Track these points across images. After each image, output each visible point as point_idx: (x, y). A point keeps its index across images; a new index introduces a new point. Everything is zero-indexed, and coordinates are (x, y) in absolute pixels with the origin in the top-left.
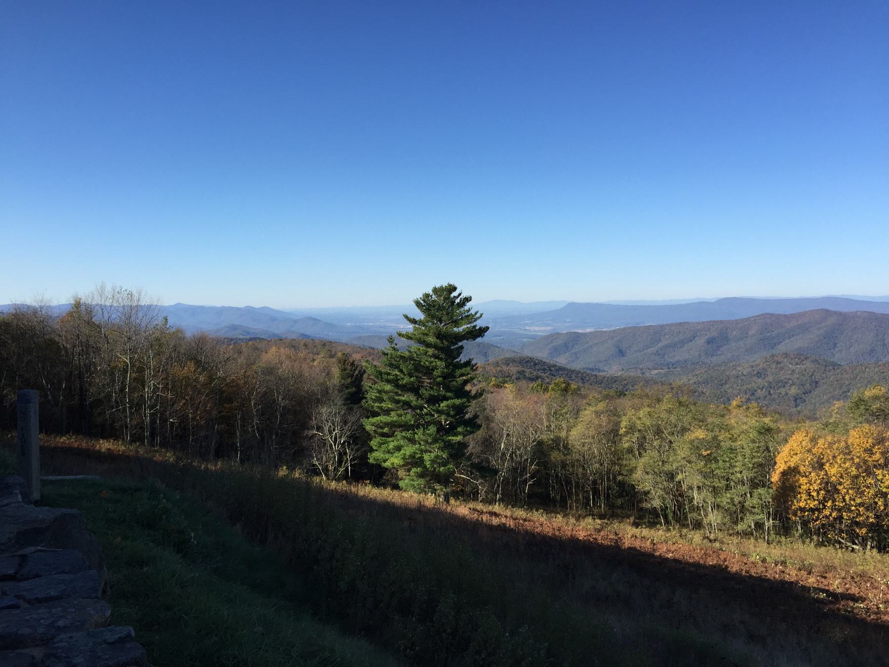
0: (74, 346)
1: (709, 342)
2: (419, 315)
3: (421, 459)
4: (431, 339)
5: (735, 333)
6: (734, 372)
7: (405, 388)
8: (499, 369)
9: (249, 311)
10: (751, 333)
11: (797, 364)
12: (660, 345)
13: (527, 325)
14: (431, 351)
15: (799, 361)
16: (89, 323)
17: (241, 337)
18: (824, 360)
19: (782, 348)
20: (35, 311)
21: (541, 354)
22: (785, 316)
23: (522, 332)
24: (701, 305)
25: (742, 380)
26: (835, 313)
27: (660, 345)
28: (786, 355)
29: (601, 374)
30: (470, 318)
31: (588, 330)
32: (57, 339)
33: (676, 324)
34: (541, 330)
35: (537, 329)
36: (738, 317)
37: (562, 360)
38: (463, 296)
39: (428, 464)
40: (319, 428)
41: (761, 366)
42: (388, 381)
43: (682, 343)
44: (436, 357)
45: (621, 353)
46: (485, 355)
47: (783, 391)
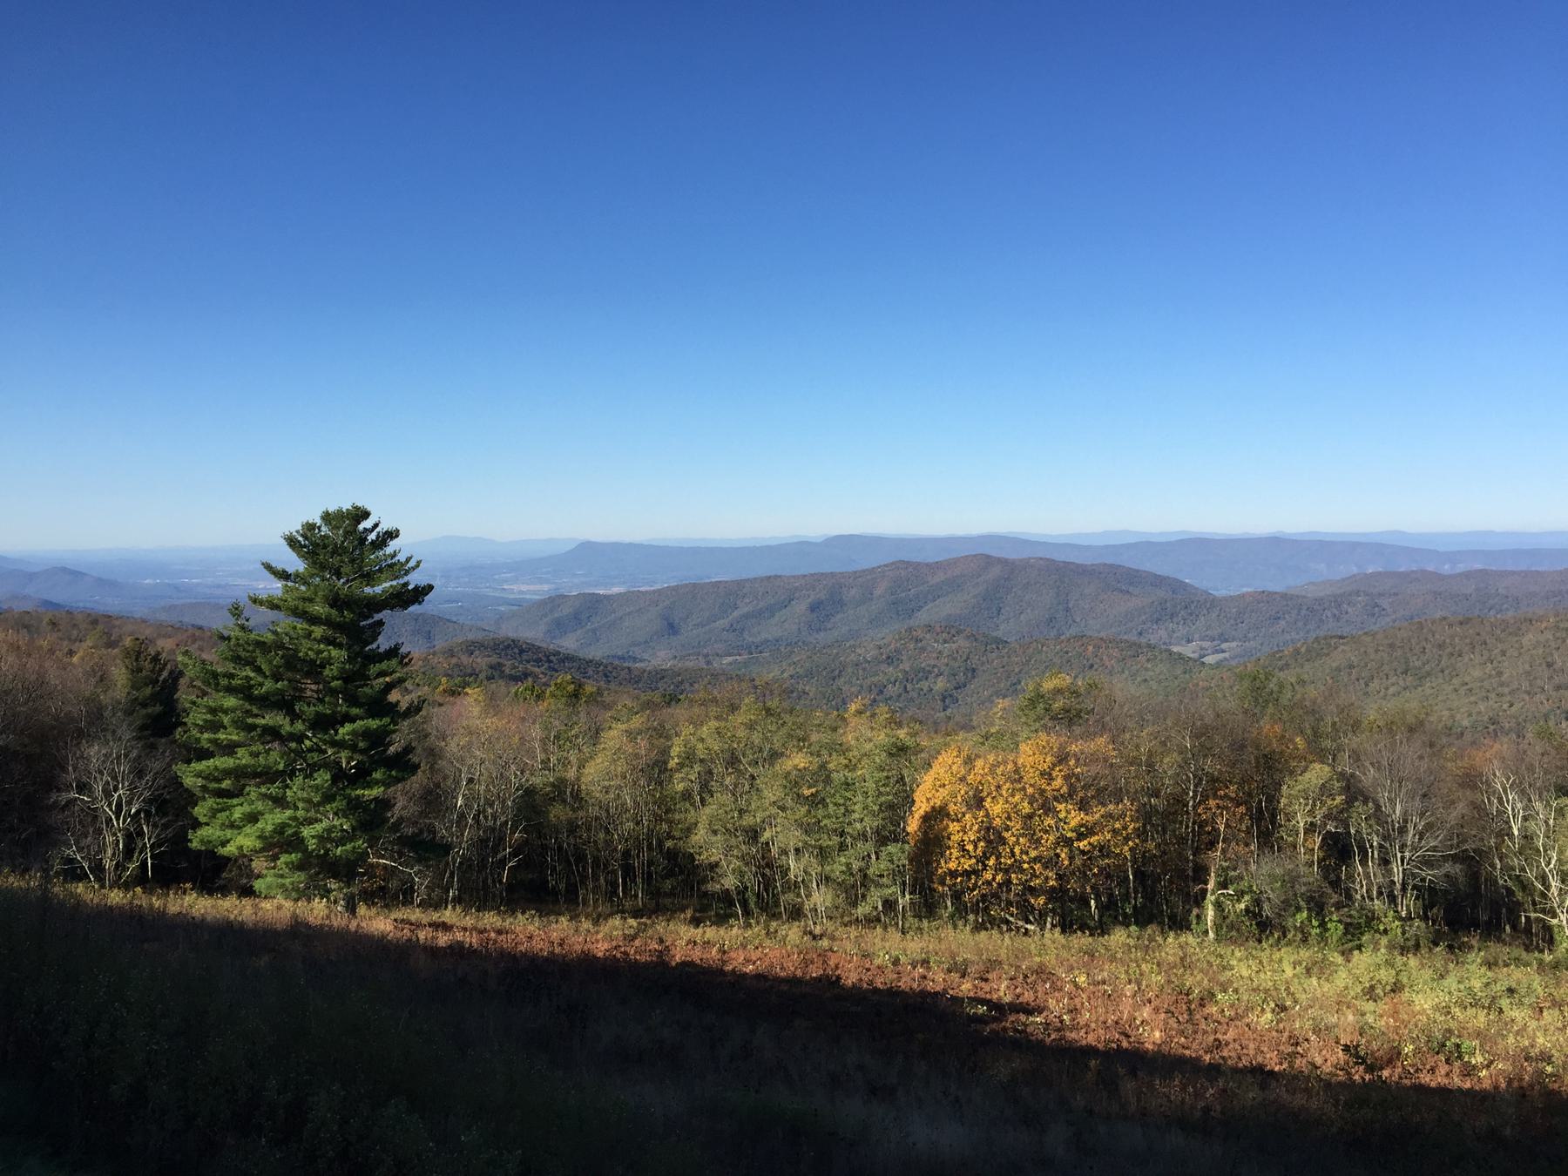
5: (853, 592)
6: (853, 657)
7: (266, 702)
8: (454, 660)
10: (877, 592)
11: (945, 642)
12: (736, 614)
13: (506, 581)
14: (318, 631)
19: (923, 617)
21: (533, 634)
24: (802, 548)
28: (929, 628)
30: (397, 568)
31: (616, 590)
33: (762, 579)
34: (532, 590)
35: (524, 588)
36: (858, 567)
37: (569, 643)
39: (312, 844)
40: (83, 788)
42: (230, 690)
43: (771, 610)
45: (672, 629)
46: (429, 636)
47: (925, 685)
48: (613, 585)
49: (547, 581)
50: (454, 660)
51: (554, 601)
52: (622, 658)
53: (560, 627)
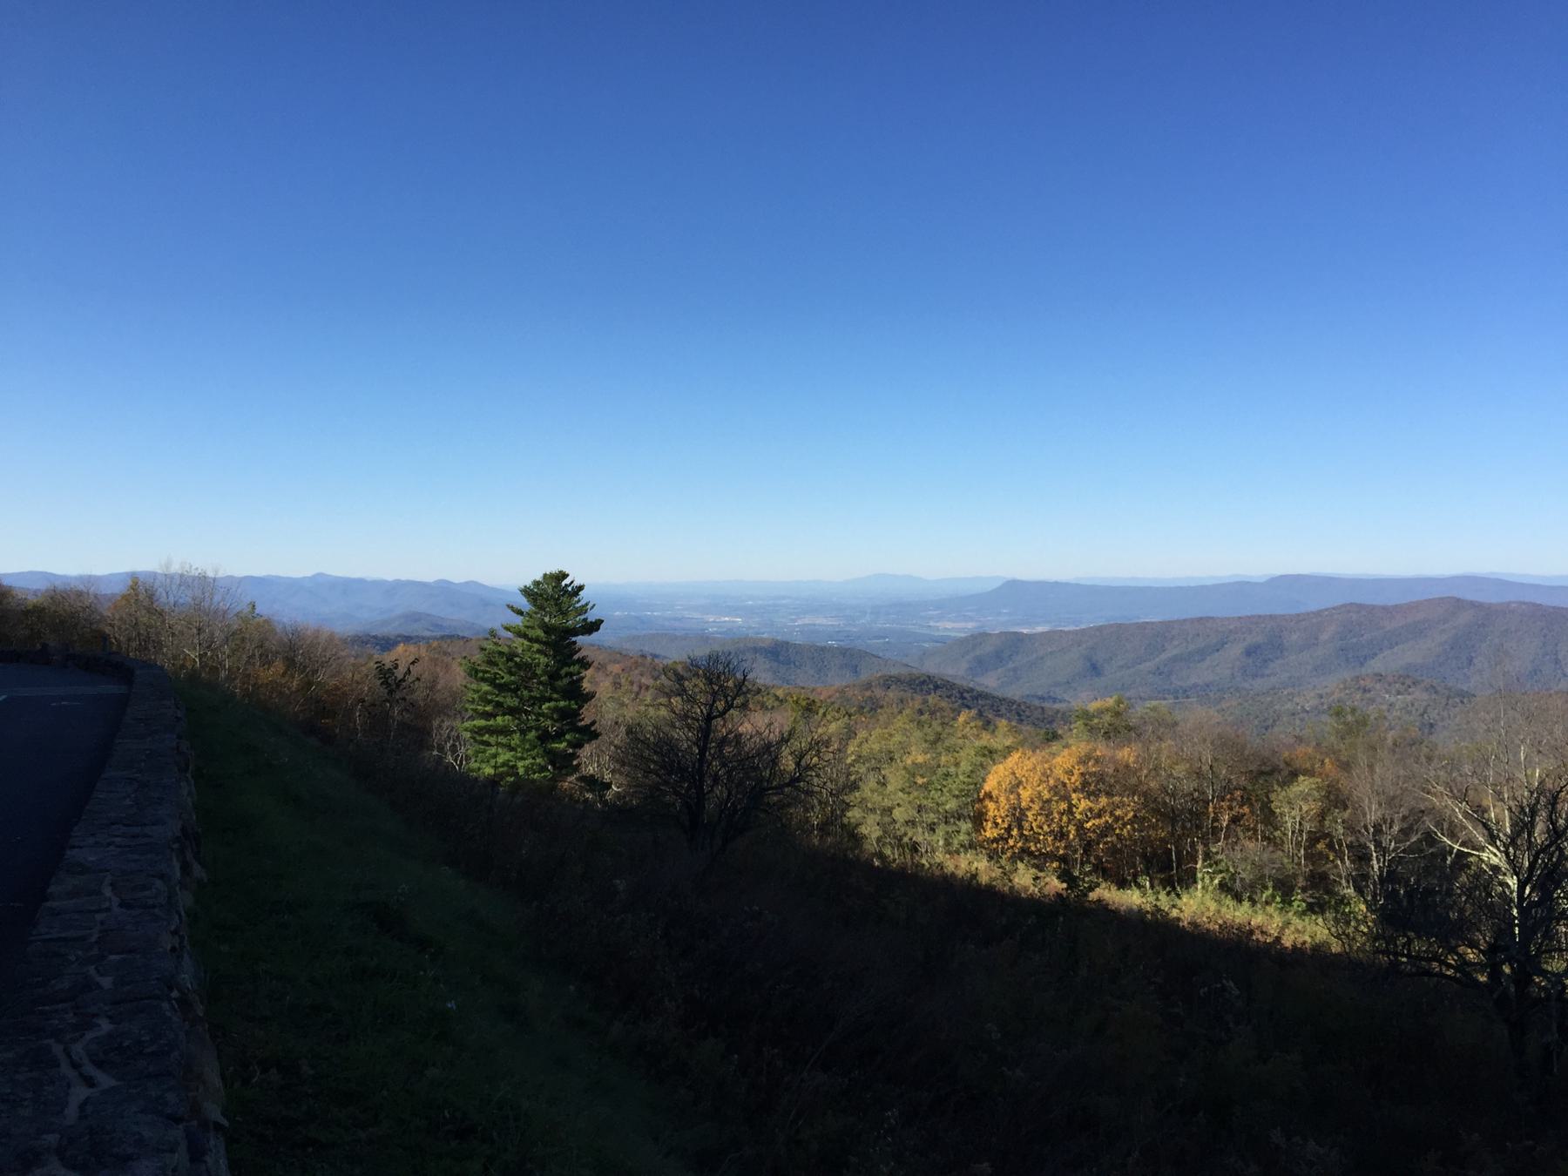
0: (129, 640)
1: (1249, 652)
2: (524, 603)
3: (514, 767)
4: (540, 633)
5: (1294, 637)
6: (1289, 706)
7: (502, 688)
8: (868, 693)
9: (444, 590)
10: (1324, 637)
11: (1399, 693)
12: (1164, 656)
13: (931, 618)
14: (536, 646)
15: (1402, 688)
16: (151, 611)
17: (428, 634)
18: (1446, 688)
19: (1376, 665)
20: (80, 594)
21: (955, 671)
22: (1385, 608)
23: (925, 631)
24: (1240, 588)
25: (1302, 720)
26: (1473, 604)
27: (1164, 656)
28: (1379, 677)
29: (1057, 706)
30: (583, 610)
31: (1040, 629)
32: (107, 630)
33: (1192, 621)
34: (954, 627)
35: (949, 625)
36: (1302, 610)
37: (990, 682)
38: (576, 584)
39: (521, 771)
40: (441, 749)
41: (1336, 696)
42: (483, 680)
43: (1202, 654)
44: (539, 651)
45: (1095, 669)
46: (855, 670)
48: (1038, 624)
49: (971, 619)
50: (868, 693)
51: (978, 639)
52: (1042, 698)
53: (981, 665)
